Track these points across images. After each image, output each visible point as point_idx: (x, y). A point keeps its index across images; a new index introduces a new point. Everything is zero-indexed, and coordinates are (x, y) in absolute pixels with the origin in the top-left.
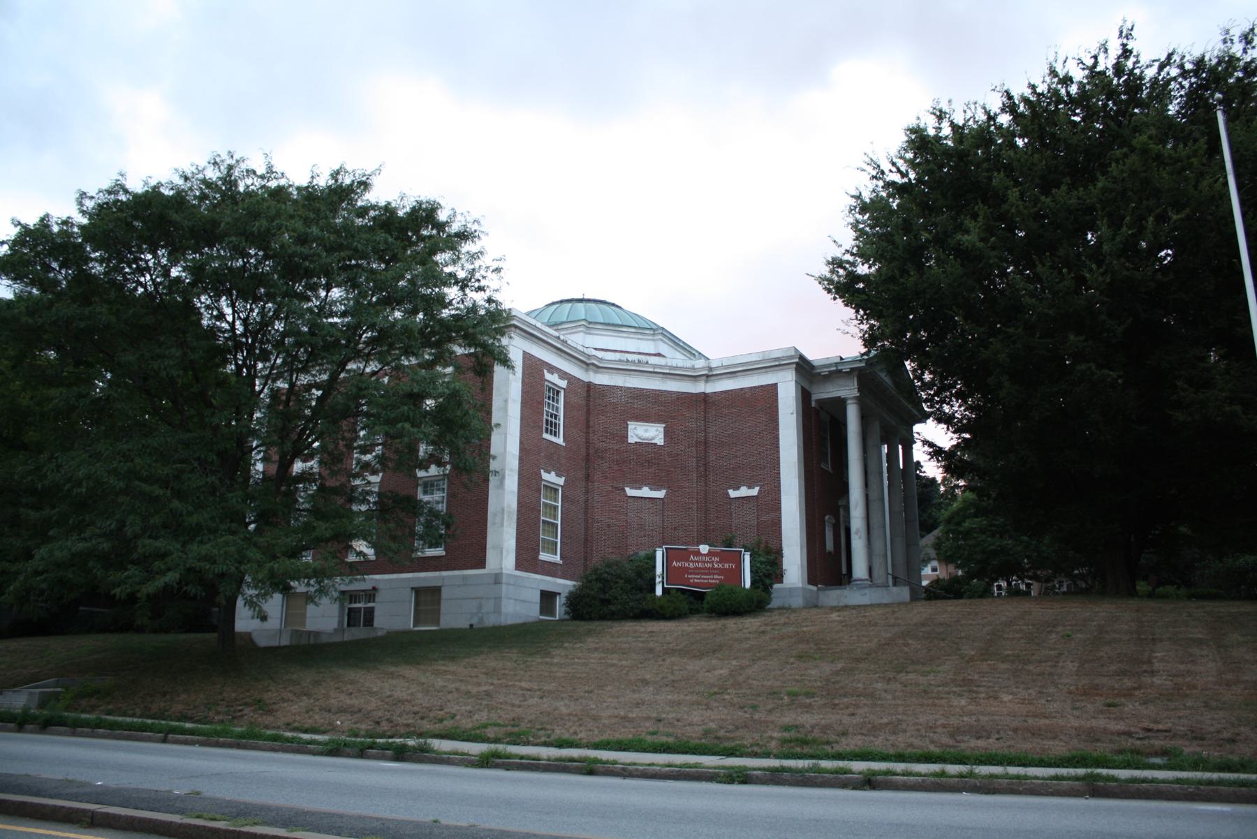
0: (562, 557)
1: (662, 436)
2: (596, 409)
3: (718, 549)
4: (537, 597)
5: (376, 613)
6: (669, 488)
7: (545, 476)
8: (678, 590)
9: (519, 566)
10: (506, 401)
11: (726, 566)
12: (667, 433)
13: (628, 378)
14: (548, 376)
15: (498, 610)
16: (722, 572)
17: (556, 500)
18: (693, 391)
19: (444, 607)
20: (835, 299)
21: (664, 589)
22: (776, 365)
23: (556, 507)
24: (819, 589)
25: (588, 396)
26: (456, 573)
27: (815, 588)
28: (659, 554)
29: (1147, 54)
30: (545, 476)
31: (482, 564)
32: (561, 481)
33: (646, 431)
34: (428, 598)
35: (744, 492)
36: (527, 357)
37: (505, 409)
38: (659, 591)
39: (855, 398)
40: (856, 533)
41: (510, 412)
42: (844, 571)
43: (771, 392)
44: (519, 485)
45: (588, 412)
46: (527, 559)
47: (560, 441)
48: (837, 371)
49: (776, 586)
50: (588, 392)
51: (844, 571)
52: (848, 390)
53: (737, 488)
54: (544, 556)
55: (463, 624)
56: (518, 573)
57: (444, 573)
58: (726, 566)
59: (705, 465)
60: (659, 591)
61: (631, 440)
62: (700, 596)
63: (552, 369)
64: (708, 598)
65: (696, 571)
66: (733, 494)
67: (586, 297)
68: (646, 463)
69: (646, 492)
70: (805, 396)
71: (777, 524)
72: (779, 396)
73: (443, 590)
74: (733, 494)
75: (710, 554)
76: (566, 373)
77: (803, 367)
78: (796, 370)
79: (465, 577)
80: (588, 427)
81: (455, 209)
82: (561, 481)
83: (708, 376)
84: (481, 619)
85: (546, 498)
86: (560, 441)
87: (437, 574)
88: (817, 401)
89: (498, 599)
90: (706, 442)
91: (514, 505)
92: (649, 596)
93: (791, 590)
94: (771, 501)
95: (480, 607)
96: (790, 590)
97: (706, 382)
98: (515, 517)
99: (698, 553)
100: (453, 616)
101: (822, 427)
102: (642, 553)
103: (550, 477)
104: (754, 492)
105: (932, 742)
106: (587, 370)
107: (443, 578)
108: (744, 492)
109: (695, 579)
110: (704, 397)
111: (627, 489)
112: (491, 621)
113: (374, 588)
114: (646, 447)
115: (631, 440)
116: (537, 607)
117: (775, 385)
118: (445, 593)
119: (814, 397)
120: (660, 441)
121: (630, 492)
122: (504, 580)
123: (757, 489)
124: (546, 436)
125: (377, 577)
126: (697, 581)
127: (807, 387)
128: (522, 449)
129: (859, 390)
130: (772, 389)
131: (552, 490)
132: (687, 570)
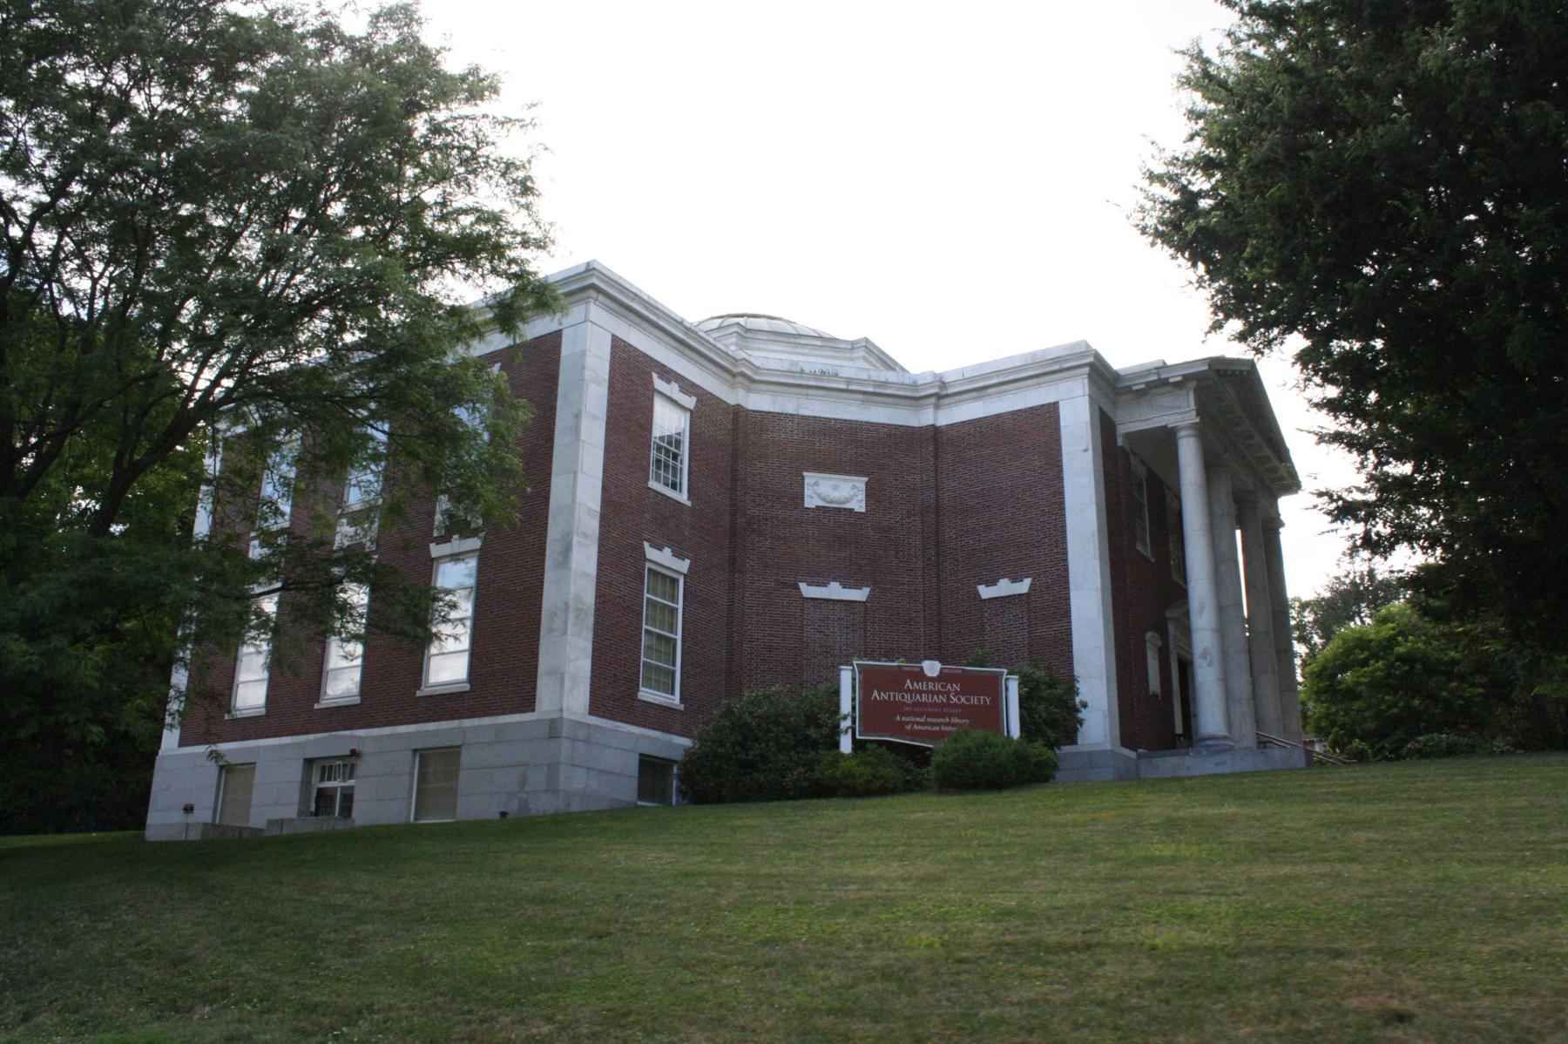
0: (683, 699)
1: (862, 496)
4: (633, 767)
5: (356, 798)
6: (875, 584)
7: (651, 553)
8: (880, 743)
9: (594, 709)
10: (577, 416)
11: (974, 700)
13: (803, 401)
14: (659, 384)
15: (552, 788)
16: (966, 711)
17: (673, 598)
18: (915, 424)
19: (464, 779)
20: (1153, 244)
21: (856, 744)
22: (1052, 368)
23: (673, 611)
24: (1139, 757)
26: (486, 721)
27: (1133, 755)
28: (846, 677)
30: (651, 553)
31: (528, 703)
32: (683, 566)
33: (835, 488)
34: (436, 764)
35: (1005, 588)
36: (618, 345)
37: (576, 429)
38: (846, 745)
39: (1193, 426)
40: (1204, 656)
41: (584, 435)
42: (1179, 730)
43: (1048, 416)
44: (600, 564)
46: (613, 691)
47: (683, 497)
48: (1159, 382)
49: (1066, 749)
51: (1179, 730)
52: (1180, 414)
53: (992, 582)
54: (646, 694)
55: (492, 813)
57: (467, 723)
58: (974, 700)
59: (938, 545)
60: (846, 745)
61: (811, 502)
62: (920, 757)
64: (936, 759)
65: (918, 709)
66: (986, 592)
70: (1105, 426)
72: (1062, 423)
73: (464, 752)
74: (986, 592)
75: (943, 677)
76: (693, 385)
77: (1100, 375)
78: (1090, 377)
79: (499, 727)
81: (454, 44)
82: (683, 566)
83: (939, 397)
85: (653, 591)
86: (683, 497)
87: (454, 724)
88: (1127, 436)
89: (553, 767)
90: (938, 508)
91: (589, 598)
92: (825, 756)
93: (1092, 757)
95: (523, 781)
96: (1090, 755)
97: (937, 407)
98: (590, 620)
99: (920, 676)
100: (477, 800)
102: (822, 687)
103: (661, 557)
104: (1023, 587)
105: (228, 1023)
106: (733, 386)
107: (464, 730)
108: (1005, 588)
109: (915, 723)
110: (935, 432)
111: (803, 586)
112: (544, 804)
113: (354, 753)
114: (834, 515)
115: (811, 502)
116: (634, 784)
117: (1054, 407)
118: (466, 758)
119: (1122, 430)
120: (858, 505)
121: (808, 591)
122: (565, 732)
123: (1027, 582)
126: (914, 731)
127: (1107, 410)
128: (606, 502)
129: (1198, 414)
130: (1048, 416)
132: (899, 707)
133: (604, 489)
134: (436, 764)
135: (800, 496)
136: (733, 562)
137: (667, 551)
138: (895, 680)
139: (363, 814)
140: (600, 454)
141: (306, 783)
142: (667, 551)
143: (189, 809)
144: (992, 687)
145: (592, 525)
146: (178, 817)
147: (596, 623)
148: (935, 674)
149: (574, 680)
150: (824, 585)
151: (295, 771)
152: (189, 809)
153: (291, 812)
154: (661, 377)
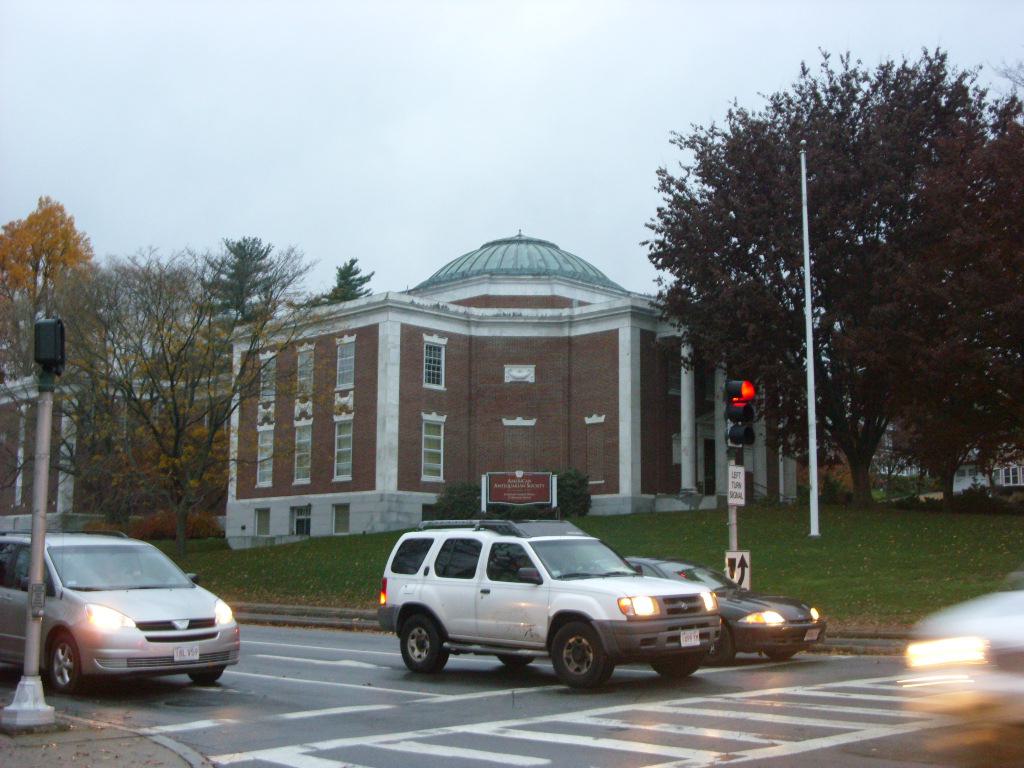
0: (445, 478)
1: (533, 374)
2: (475, 360)
3: (531, 473)
5: (312, 523)
6: (540, 418)
7: (426, 417)
9: (401, 487)
11: (537, 486)
12: (537, 372)
23: (439, 441)
25: (470, 349)
27: (652, 496)
28: (484, 480)
29: (758, 108)
31: (372, 487)
32: (443, 419)
33: (520, 372)
34: (342, 509)
41: (389, 373)
45: (470, 361)
46: (409, 478)
47: (441, 387)
50: (470, 343)
53: (590, 416)
56: (401, 493)
57: (352, 494)
61: (508, 379)
63: (431, 332)
65: (513, 491)
66: (588, 421)
67: (527, 234)
68: (520, 398)
69: (519, 422)
71: (615, 446)
74: (588, 421)
79: (364, 497)
80: (470, 372)
82: (443, 419)
84: (373, 528)
85: (426, 433)
88: (660, 339)
91: (395, 442)
94: (611, 428)
99: (514, 477)
101: (657, 362)
104: (602, 419)
110: (569, 341)
114: (519, 384)
115: (508, 379)
119: (658, 336)
120: (531, 379)
121: (507, 422)
123: (604, 417)
124: (427, 385)
125: (312, 496)
131: (435, 427)
132: (506, 490)
133: (401, 394)
134: (342, 509)
135: (503, 378)
136: (470, 411)
137: (434, 414)
138: (504, 479)
139: (697, 632)
140: (397, 379)
141: (292, 517)
142: (434, 414)
143: (243, 528)
144: (546, 480)
145: (395, 411)
146: (239, 532)
147: (400, 452)
148: (520, 476)
149: (390, 478)
150: (515, 419)
151: (287, 512)
152: (243, 528)
153: (286, 532)
154: (427, 334)
